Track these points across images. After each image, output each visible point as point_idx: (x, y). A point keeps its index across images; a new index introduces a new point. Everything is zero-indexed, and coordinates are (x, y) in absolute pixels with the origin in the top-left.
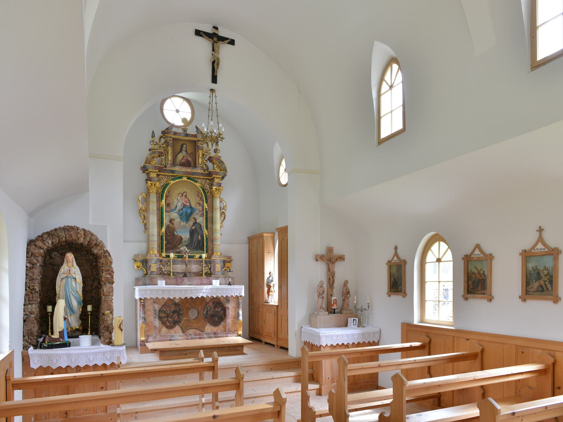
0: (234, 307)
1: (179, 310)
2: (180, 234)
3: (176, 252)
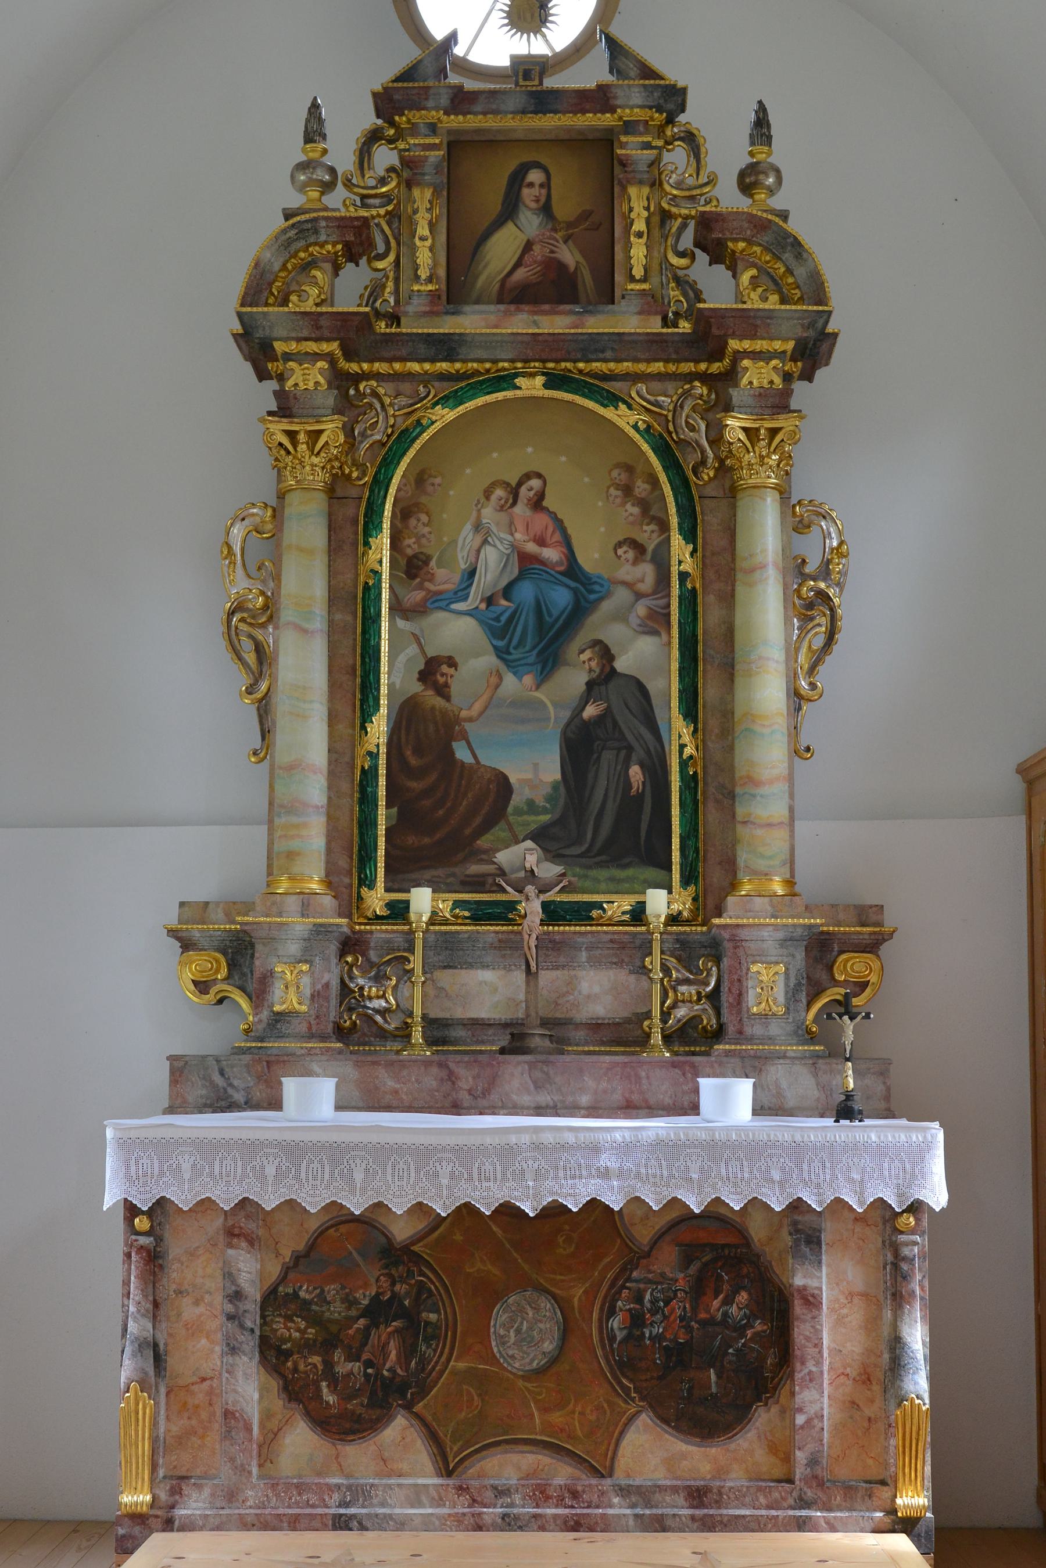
0: (864, 1295)
1: (417, 1301)
2: (492, 758)
3: (463, 883)
